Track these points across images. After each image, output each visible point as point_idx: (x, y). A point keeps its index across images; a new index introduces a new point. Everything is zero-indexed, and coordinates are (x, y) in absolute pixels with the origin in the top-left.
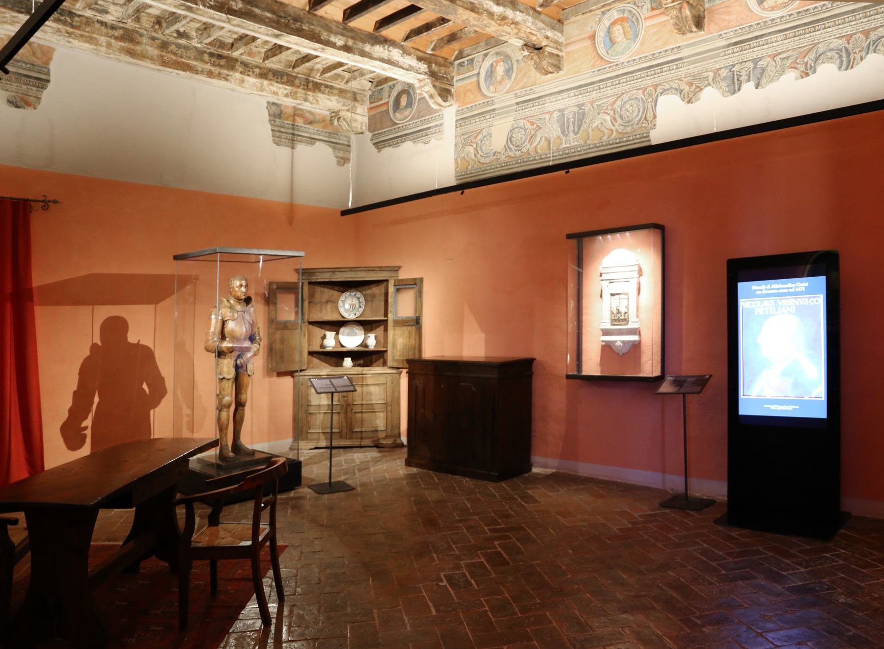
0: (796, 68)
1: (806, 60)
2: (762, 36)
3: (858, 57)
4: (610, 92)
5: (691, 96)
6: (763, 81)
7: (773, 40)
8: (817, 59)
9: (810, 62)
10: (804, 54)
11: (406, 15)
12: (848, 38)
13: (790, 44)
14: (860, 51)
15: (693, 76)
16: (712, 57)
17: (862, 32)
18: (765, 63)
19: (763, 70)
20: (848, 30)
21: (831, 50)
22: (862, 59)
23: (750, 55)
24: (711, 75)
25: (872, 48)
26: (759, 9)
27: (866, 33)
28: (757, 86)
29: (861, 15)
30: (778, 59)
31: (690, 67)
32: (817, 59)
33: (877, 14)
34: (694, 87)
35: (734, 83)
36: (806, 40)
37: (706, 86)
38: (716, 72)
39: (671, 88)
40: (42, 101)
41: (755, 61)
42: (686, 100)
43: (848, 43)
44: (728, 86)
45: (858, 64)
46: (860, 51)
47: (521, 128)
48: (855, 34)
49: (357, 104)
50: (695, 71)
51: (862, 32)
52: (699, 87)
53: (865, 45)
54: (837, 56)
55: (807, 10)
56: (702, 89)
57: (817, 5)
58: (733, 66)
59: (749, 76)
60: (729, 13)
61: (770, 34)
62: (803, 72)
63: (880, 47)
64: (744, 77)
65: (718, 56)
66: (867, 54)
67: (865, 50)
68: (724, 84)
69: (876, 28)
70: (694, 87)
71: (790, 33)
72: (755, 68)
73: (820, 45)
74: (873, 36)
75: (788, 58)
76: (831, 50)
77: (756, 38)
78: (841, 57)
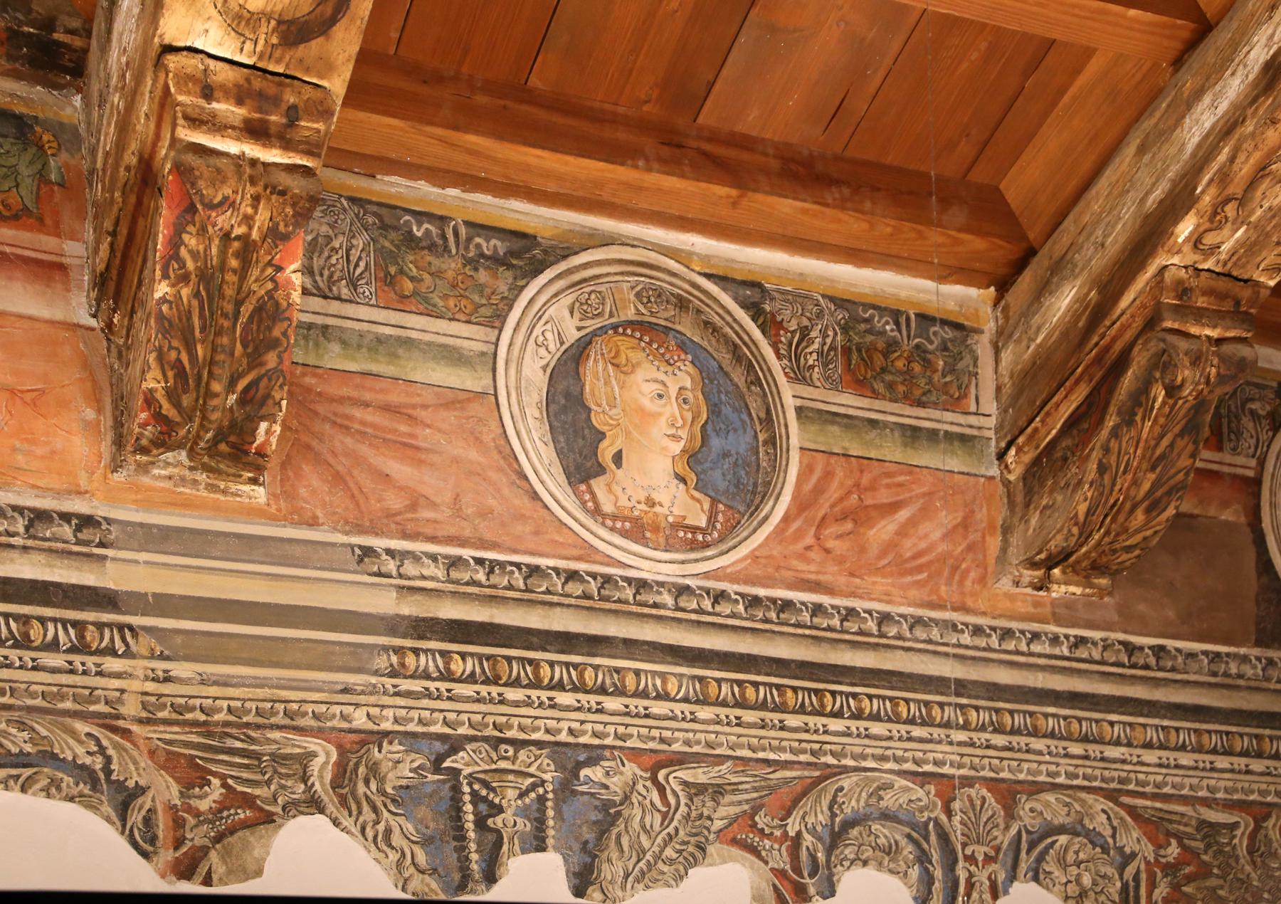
0: (754, 851)
1: (793, 827)
2: (595, 644)
3: (982, 877)
5: (197, 836)
6: (611, 868)
8: (836, 838)
9: (808, 840)
10: (785, 795)
12: (947, 788)
13: (707, 727)
14: (989, 859)
15: (205, 728)
16: (324, 659)
18: (616, 783)
19: (608, 816)
20: (945, 755)
21: (886, 816)
23: (568, 717)
24: (324, 757)
26: (571, 503)
27: (1008, 793)
28: (582, 881)
29: (985, 716)
30: (674, 778)
31: (181, 669)
32: (836, 838)
33: (1035, 733)
34: (215, 791)
35: (461, 837)
36: (791, 737)
37: (293, 808)
38: (356, 749)
39: (51, 758)
40: (685, 883)
41: (573, 759)
43: (949, 813)
44: (426, 842)
46: (989, 859)
50: (222, 702)
52: (248, 801)
53: (1005, 840)
54: (908, 850)
55: (787, 605)
56: (268, 819)
58: (455, 745)
59: (540, 823)
60: (410, 450)
61: (630, 647)
62: (779, 873)
64: (510, 821)
65: (356, 660)
66: (1012, 877)
67: (1005, 857)
68: (403, 827)
70: (215, 791)
71: (720, 679)
72: (566, 789)
73: (847, 782)
74: (1029, 812)
75: (718, 791)
76: (886, 816)
77: (567, 641)
78: (923, 858)
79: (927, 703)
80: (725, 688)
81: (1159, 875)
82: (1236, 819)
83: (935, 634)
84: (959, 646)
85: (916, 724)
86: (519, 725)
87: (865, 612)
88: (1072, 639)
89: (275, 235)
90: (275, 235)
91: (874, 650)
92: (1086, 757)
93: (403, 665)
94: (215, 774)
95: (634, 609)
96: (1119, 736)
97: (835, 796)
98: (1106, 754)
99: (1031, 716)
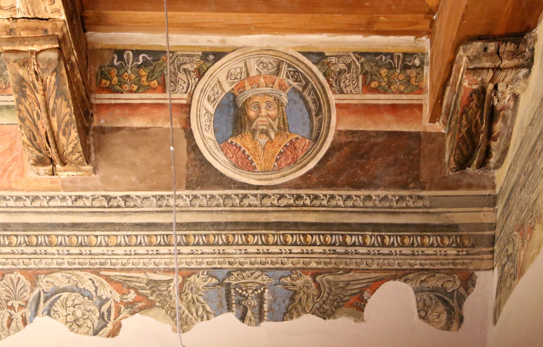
4: (166, 259)
7: (120, 239)
11: (294, 32)
17: (24, 271)
22: (25, 323)
25: (43, 307)
27: (33, 276)
33: (50, 245)
42: (199, 320)
45: (18, 329)
46: (21, 307)
47: (184, 281)
48: (11, 271)
49: (192, 153)
51: (24, 271)
53: (31, 297)
57: (216, 193)
63: (58, 307)
66: (35, 314)
69: (50, 271)
74: (44, 284)
81: (123, 308)
84: (42, 207)
86: (398, 263)
87: (9, 196)
88: (208, 196)
99: (440, 237)
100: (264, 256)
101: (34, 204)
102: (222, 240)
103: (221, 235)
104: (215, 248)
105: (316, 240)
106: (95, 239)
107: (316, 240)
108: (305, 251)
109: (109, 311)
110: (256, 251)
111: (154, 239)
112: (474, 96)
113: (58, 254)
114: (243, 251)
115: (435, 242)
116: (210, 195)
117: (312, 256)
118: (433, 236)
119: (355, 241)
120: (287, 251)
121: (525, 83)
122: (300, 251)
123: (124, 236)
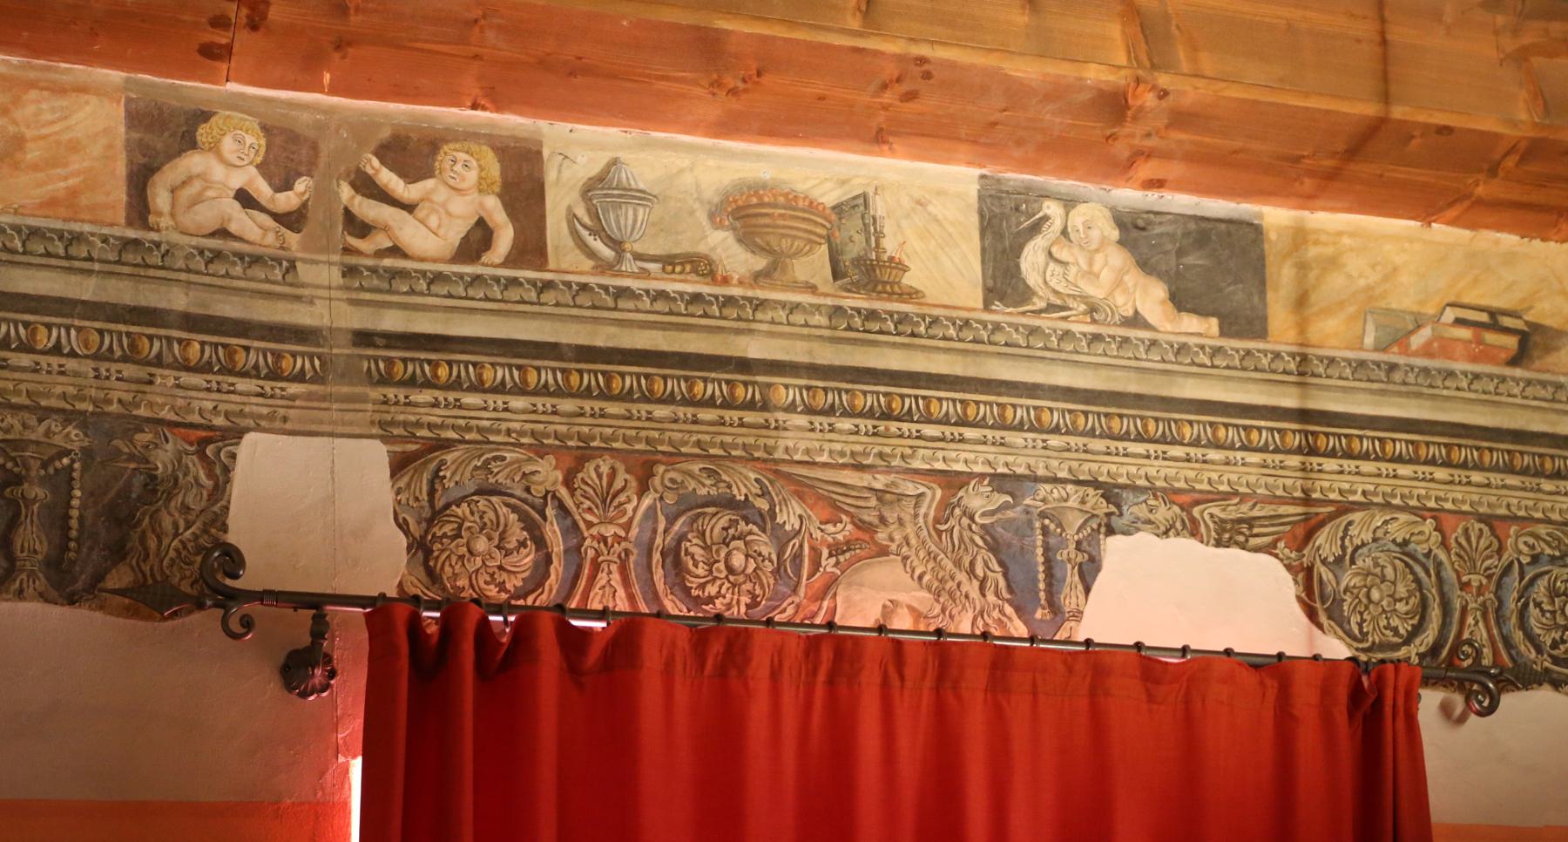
61: (1033, 390)
73: (1357, 516)
79: (1541, 456)
80: (1289, 438)
81: (825, 553)
82: (922, 489)
83: (781, 315)
85: (1094, 436)
89: (1154, 88)
90: (1154, 88)
91: (664, 329)
92: (1488, 485)
93: (435, 376)
94: (847, 513)
95: (787, 329)
96: (872, 407)
97: (1346, 530)
98: (1248, 460)
100: (993, 449)
101: (212, 268)
102: (121, 346)
103: (68, 329)
104: (943, 428)
105: (59, 336)
106: (244, 354)
107: (59, 336)
108: (541, 408)
109: (797, 557)
110: (205, 385)
111: (1254, 435)
112: (1121, 150)
113: (96, 377)
114: (1041, 444)
115: (717, 393)
116: (578, 284)
117: (1280, 472)
118: (502, 365)
119: (459, 376)
120: (644, 414)
121: (1135, 118)
122: (1336, 468)
123: (801, 388)
